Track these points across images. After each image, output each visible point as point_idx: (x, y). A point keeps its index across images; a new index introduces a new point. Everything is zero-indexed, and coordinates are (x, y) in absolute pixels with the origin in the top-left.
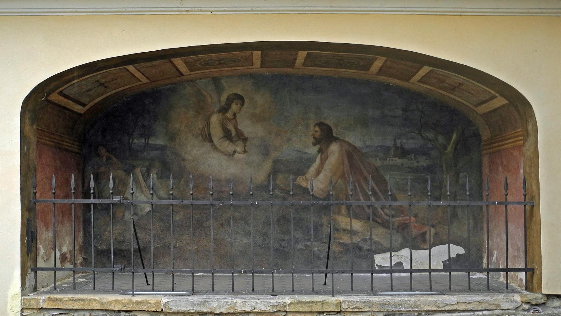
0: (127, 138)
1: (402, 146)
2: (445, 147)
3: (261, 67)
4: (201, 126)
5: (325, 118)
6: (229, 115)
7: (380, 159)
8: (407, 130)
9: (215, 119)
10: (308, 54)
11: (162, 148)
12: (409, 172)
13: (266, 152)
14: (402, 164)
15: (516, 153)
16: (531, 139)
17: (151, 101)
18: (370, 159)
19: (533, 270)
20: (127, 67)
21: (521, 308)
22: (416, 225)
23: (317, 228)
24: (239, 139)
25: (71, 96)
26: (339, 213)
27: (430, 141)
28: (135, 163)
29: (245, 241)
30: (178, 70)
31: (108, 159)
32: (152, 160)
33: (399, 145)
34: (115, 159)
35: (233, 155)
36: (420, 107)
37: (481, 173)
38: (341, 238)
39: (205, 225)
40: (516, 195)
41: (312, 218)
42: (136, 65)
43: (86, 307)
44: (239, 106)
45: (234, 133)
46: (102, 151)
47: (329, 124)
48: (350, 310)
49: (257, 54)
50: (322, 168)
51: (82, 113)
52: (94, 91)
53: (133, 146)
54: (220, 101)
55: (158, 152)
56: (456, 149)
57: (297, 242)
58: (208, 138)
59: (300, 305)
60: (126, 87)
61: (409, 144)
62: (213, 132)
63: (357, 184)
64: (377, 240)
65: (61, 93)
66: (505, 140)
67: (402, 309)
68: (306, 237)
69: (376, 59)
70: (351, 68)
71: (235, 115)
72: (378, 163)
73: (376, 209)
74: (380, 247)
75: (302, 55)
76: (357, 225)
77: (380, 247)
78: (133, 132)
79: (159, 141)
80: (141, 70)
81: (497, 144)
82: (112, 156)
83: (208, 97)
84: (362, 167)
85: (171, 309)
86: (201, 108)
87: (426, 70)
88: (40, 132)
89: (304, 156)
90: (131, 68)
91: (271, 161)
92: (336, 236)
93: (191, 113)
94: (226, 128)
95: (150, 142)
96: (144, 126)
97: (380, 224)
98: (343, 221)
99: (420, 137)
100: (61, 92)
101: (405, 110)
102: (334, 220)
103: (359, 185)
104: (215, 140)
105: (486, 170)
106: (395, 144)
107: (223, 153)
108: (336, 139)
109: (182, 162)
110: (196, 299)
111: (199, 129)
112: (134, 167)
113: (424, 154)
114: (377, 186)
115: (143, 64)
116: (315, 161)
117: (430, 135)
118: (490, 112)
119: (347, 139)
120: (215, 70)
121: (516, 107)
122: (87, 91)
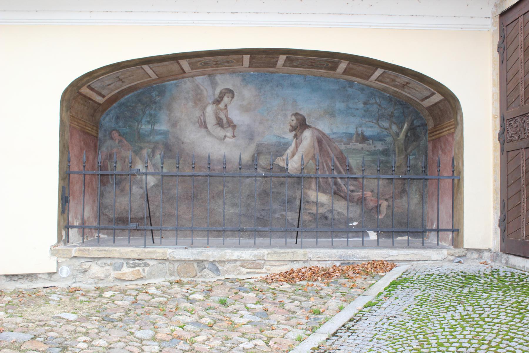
0: (136, 124)
1: (362, 133)
2: (398, 135)
3: (249, 67)
4: (198, 115)
5: (300, 109)
6: (222, 106)
7: (344, 144)
8: (367, 120)
9: (210, 110)
10: (287, 57)
11: (165, 133)
12: (368, 155)
13: (251, 136)
14: (362, 148)
15: (450, 139)
16: (459, 127)
17: (157, 94)
18: (336, 143)
19: (458, 230)
20: (143, 66)
21: (447, 260)
22: (372, 198)
23: (290, 201)
24: (229, 126)
25: (96, 89)
26: (310, 188)
27: (386, 129)
28: (142, 145)
29: (232, 211)
30: (182, 69)
31: (120, 141)
32: (157, 143)
33: (360, 132)
34: (126, 142)
35: (224, 139)
36: (378, 101)
37: (426, 156)
38: (311, 209)
39: (199, 197)
40: (446, 172)
41: (287, 192)
42: (150, 65)
43: (108, 256)
44: (230, 99)
45: (225, 120)
46: (115, 135)
47: (303, 115)
48: (315, 259)
49: (247, 58)
50: (297, 150)
51: (101, 103)
52: (113, 85)
53: (141, 131)
54: (214, 95)
55: (162, 136)
56: (406, 136)
57: (275, 212)
58: (204, 125)
59: (276, 255)
60: (138, 82)
61: (368, 132)
62: (208, 121)
63: (325, 164)
64: (340, 211)
65: (89, 87)
66: (444, 128)
67: (355, 259)
68: (282, 208)
69: (340, 62)
70: (321, 68)
71: (226, 106)
72: (343, 147)
73: (340, 185)
74: (342, 216)
75: (282, 58)
76: (323, 198)
77: (342, 216)
78: (142, 119)
79: (162, 127)
80: (153, 69)
81: (438, 132)
82: (124, 140)
83: (205, 91)
84: (330, 151)
85: (175, 258)
86: (198, 99)
87: (379, 72)
88: (72, 118)
89: (282, 140)
90: (146, 67)
91: (255, 144)
92: (307, 207)
93: (191, 104)
94: (219, 117)
95: (156, 128)
96: (151, 115)
97: (342, 197)
98: (312, 195)
99: (377, 126)
100: (89, 85)
101: (365, 103)
102: (306, 194)
103: (326, 165)
104: (209, 126)
105: (430, 153)
106: (357, 132)
107: (215, 137)
108: (308, 127)
109: (182, 145)
110: (195, 251)
111: (196, 117)
112: (141, 148)
113: (380, 140)
114: (341, 166)
115: (156, 65)
116: (291, 145)
117: (386, 124)
118: (432, 106)
119: (317, 127)
120: (212, 69)
121: (449, 102)
122: (108, 85)
